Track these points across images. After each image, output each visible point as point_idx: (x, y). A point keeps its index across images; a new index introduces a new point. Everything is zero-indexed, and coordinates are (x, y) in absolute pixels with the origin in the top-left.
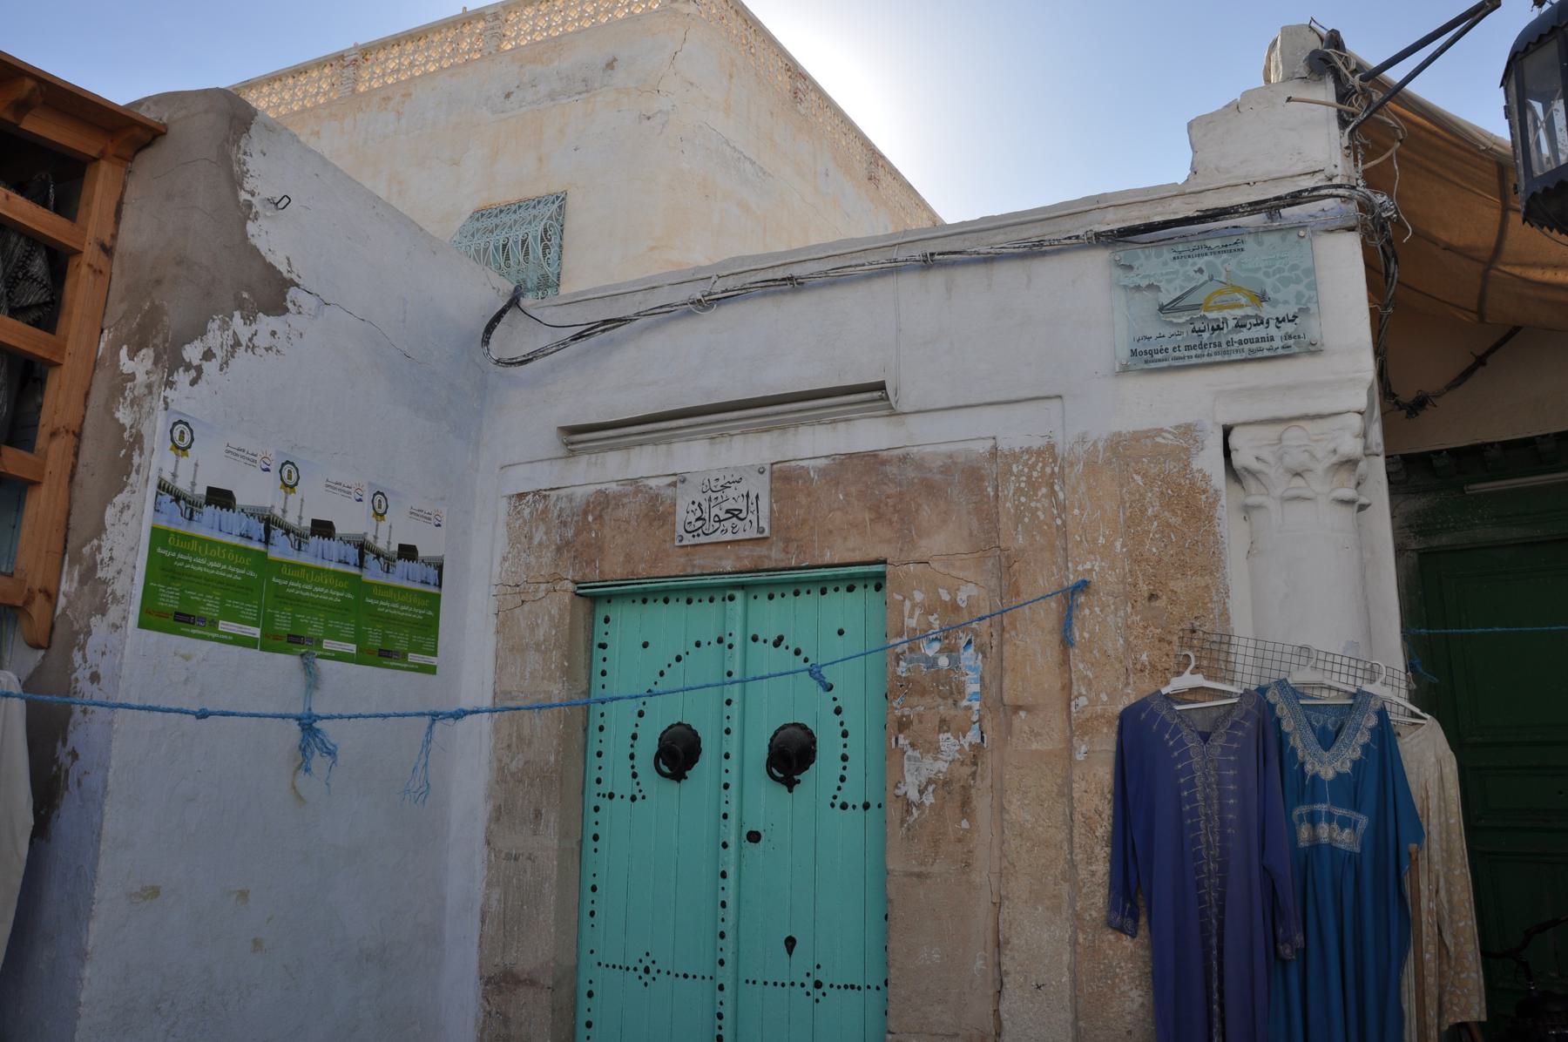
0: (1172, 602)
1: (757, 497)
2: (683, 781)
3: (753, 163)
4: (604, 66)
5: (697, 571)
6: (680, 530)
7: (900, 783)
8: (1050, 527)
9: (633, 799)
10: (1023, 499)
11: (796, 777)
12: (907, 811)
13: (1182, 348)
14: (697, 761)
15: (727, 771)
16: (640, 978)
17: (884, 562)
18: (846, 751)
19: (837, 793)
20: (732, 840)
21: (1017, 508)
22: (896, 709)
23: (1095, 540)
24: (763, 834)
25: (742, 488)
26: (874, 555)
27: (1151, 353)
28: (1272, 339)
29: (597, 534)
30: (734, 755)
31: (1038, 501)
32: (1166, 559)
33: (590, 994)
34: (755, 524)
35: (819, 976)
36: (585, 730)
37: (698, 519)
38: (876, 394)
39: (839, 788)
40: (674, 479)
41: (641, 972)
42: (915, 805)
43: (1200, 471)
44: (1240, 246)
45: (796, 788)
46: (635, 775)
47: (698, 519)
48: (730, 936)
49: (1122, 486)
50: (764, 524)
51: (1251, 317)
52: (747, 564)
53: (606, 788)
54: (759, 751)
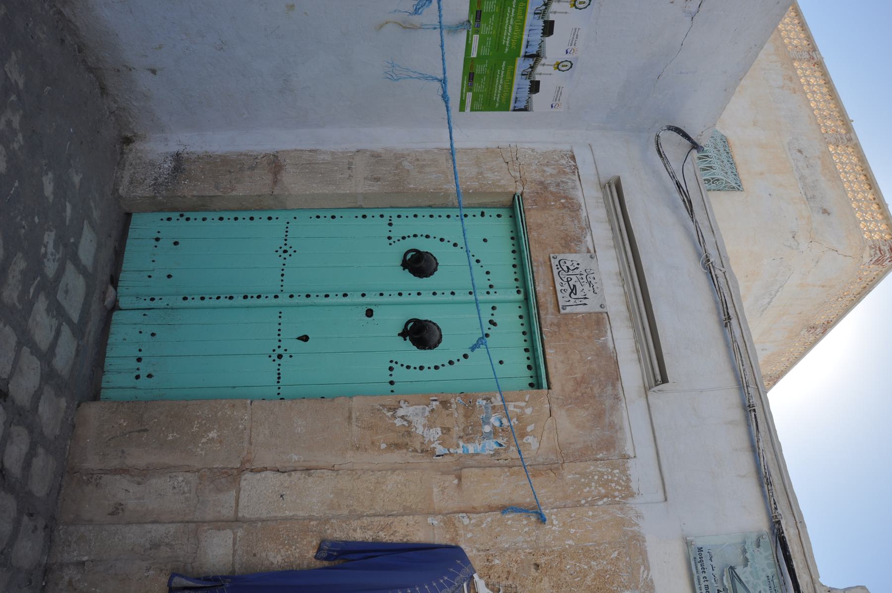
0: (534, 579)
1: (585, 304)
2: (402, 268)
3: (769, 303)
4: (825, 207)
7: (408, 403)
8: (579, 496)
9: (389, 238)
10: (596, 477)
11: (408, 338)
12: (390, 408)
13: (706, 583)
14: (414, 276)
17: (549, 388)
18: (426, 369)
19: (399, 364)
21: (590, 473)
22: (455, 399)
23: (572, 526)
24: (371, 318)
25: (590, 295)
29: (552, 205)
30: (419, 298)
31: (596, 487)
32: (563, 575)
33: (270, 218)
34: (568, 304)
35: (286, 357)
36: (430, 207)
38: (659, 378)
39: (402, 365)
40: (592, 251)
41: (284, 248)
42: (394, 413)
45: (401, 338)
46: (404, 238)
49: (609, 543)
50: (568, 309)
53: (395, 221)
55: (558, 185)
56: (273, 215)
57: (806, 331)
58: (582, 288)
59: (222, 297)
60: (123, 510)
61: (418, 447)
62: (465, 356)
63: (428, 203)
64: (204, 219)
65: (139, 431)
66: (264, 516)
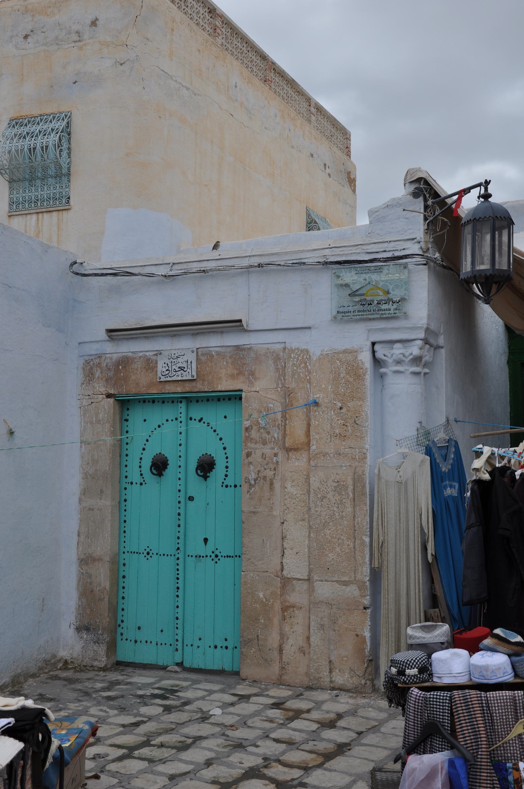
0: (348, 411)
1: (191, 362)
3: (188, 89)
4: (90, 23)
5: (167, 392)
6: (159, 374)
8: (305, 379)
9: (141, 484)
10: (295, 368)
11: (208, 475)
13: (356, 311)
15: (180, 472)
16: (145, 556)
17: (242, 391)
18: (227, 464)
20: (182, 499)
21: (293, 371)
23: (321, 386)
25: (185, 358)
26: (238, 388)
27: (344, 313)
28: (390, 310)
29: (124, 375)
31: (301, 369)
32: (347, 394)
33: (124, 565)
34: (190, 373)
35: (217, 552)
36: (120, 456)
37: (167, 370)
38: (238, 324)
40: (156, 352)
41: (145, 554)
43: (361, 360)
44: (381, 270)
45: (208, 479)
46: (141, 475)
47: (167, 370)
48: (182, 526)
49: (332, 365)
50: (194, 373)
51: (383, 300)
52: (188, 389)
53: (129, 480)
54: (193, 464)
55: (109, 369)
56: (122, 562)
57: (218, 38)
58: (180, 363)
59: (177, 594)
60: (303, 647)
61: (273, 473)
62: (221, 439)
63: (118, 458)
64: (123, 610)
65: (258, 640)
66: (308, 564)
